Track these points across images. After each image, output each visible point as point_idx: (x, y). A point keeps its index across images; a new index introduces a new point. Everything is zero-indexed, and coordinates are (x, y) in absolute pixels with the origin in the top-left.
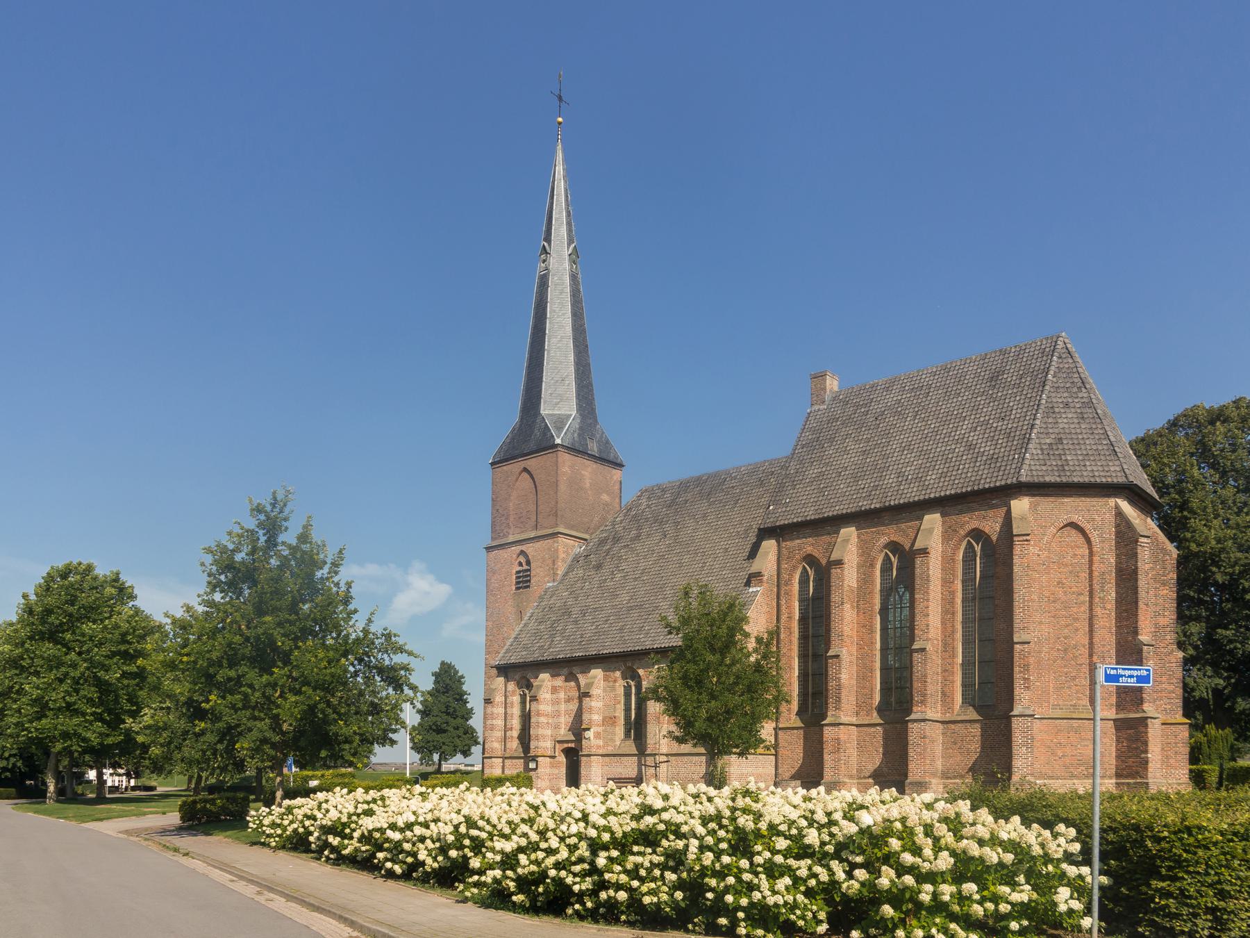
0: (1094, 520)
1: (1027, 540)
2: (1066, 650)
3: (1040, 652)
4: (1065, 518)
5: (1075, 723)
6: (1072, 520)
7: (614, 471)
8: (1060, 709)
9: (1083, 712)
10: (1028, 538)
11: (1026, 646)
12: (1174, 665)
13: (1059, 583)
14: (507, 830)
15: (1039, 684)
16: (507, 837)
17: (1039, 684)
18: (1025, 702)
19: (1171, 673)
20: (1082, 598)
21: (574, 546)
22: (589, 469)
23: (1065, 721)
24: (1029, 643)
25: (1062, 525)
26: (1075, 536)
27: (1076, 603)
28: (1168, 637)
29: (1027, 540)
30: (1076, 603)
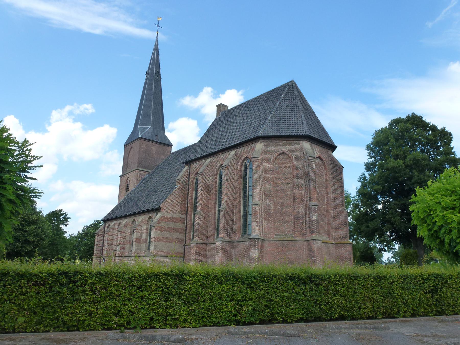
0: (293, 151)
1: (258, 160)
2: (282, 209)
3: (269, 210)
4: (280, 151)
5: (286, 243)
6: (284, 151)
7: (168, 147)
8: (279, 236)
9: (289, 238)
10: (258, 159)
11: (257, 206)
12: (343, 216)
13: (279, 179)
14: (11, 294)
15: (269, 224)
16: (12, 295)
17: (269, 224)
18: (256, 233)
19: (342, 220)
20: (289, 185)
21: (145, 175)
22: (155, 147)
23: (281, 241)
24: (258, 205)
25: (279, 153)
26: (282, 156)
27: (287, 188)
28: (340, 204)
29: (258, 160)
30: (287, 188)
